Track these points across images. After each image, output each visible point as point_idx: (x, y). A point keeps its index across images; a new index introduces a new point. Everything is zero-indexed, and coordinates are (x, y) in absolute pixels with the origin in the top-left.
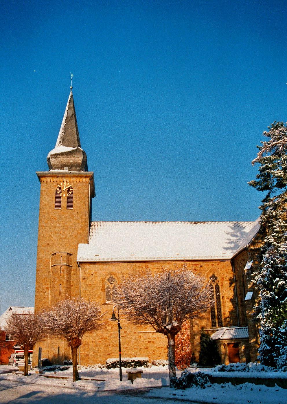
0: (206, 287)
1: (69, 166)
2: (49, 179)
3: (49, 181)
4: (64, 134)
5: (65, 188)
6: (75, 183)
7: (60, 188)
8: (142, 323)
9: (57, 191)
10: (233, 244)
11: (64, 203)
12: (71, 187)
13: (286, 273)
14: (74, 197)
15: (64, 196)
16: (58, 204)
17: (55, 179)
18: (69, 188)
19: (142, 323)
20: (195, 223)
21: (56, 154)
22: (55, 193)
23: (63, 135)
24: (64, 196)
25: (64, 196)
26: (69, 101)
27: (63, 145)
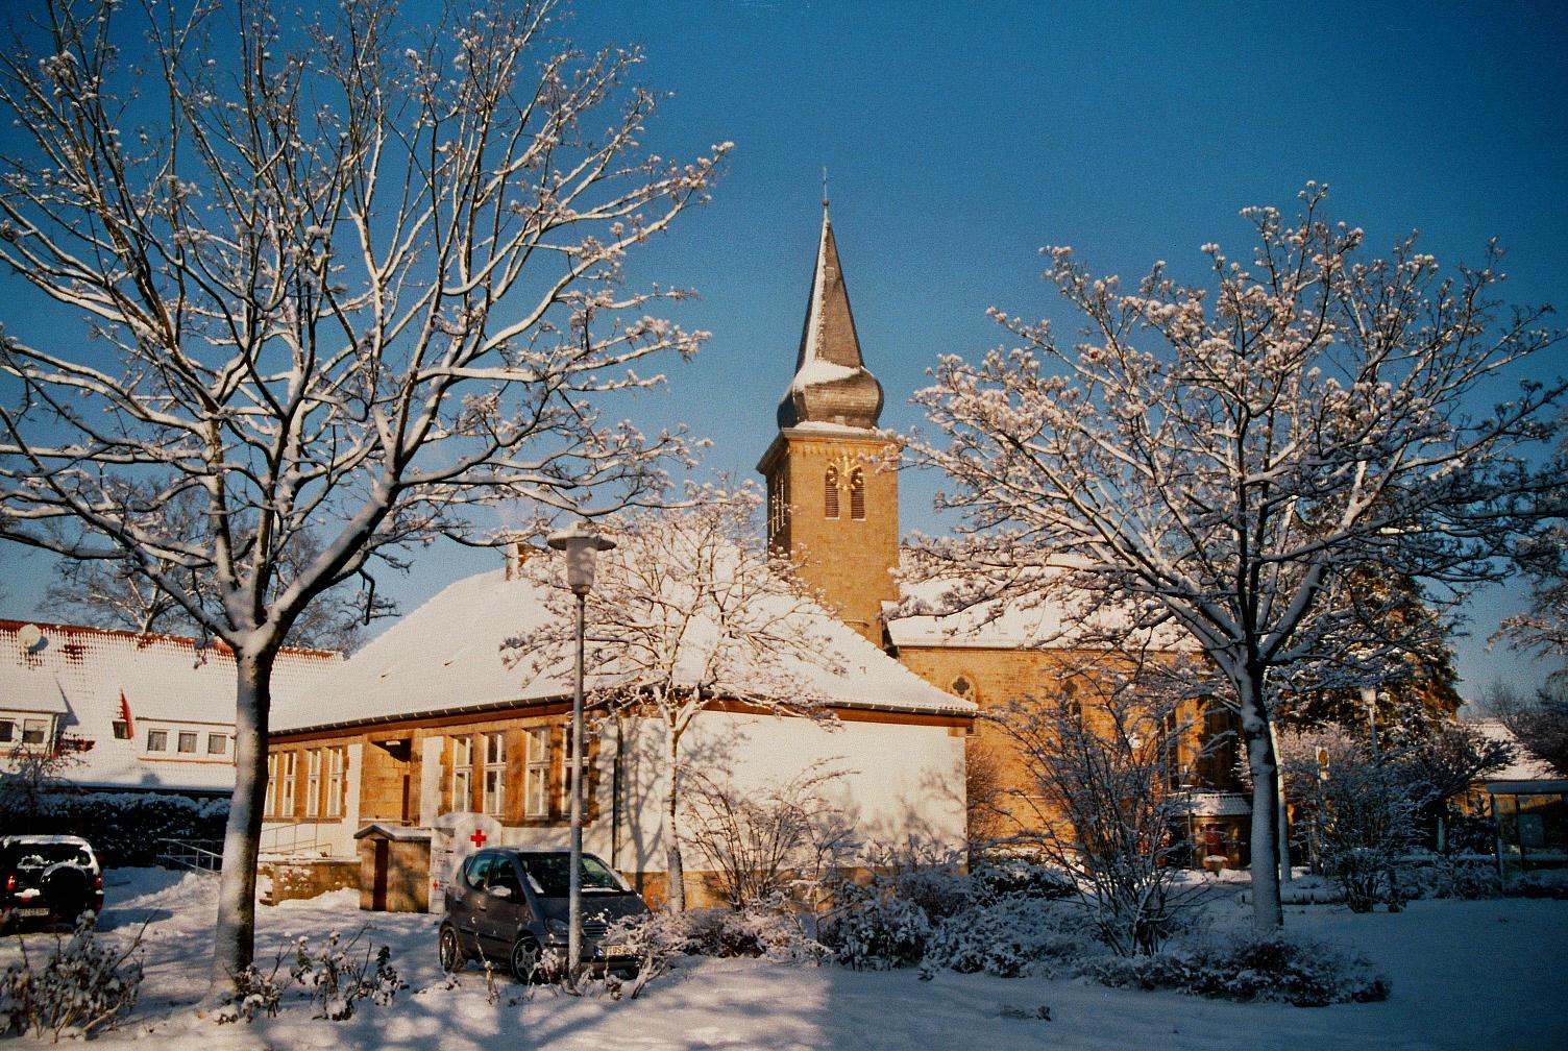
2: (809, 447)
4: (825, 328)
5: (847, 472)
7: (835, 470)
9: (828, 477)
11: (845, 505)
12: (860, 470)
14: (866, 492)
16: (832, 508)
17: (822, 447)
24: (845, 488)
25: (845, 488)
26: (827, 239)
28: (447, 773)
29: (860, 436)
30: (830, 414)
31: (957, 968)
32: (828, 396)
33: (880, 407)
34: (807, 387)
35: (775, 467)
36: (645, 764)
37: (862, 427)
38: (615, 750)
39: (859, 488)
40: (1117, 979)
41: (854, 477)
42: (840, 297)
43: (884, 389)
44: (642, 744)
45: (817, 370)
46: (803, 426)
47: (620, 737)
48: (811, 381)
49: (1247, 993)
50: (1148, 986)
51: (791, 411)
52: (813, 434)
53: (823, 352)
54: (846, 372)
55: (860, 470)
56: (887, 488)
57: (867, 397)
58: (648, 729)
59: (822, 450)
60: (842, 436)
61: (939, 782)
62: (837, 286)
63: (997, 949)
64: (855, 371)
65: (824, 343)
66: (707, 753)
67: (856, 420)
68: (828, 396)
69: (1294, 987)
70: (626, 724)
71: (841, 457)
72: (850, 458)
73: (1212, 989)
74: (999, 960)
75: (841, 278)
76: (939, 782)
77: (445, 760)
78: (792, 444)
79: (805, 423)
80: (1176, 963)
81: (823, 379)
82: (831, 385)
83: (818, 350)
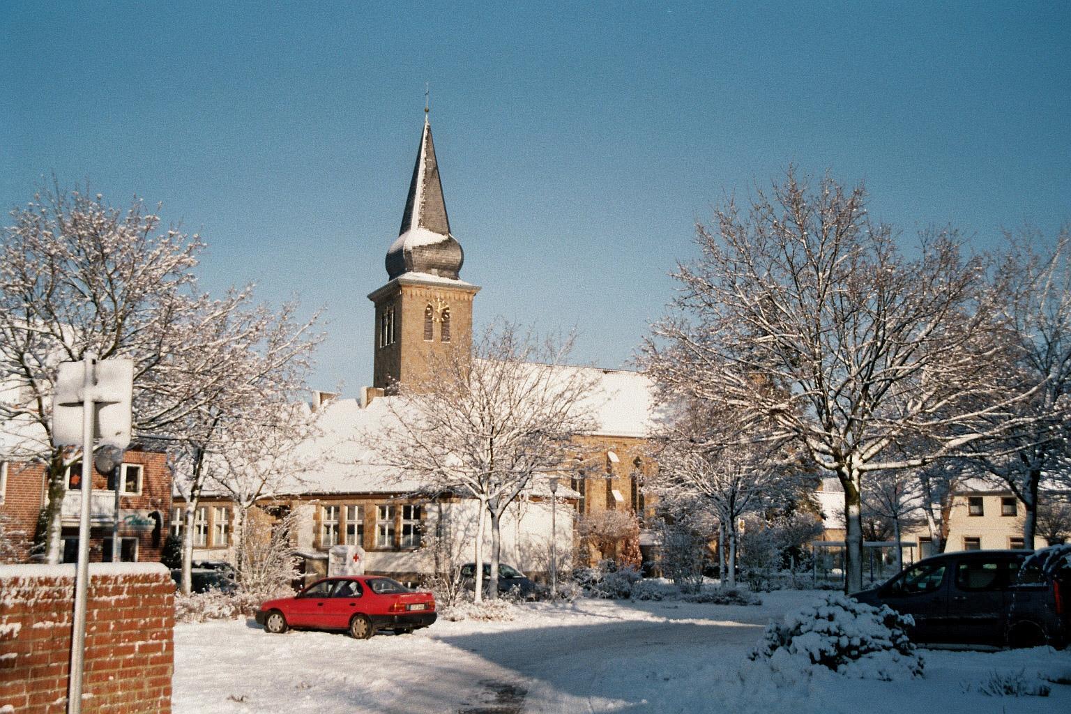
0: (273, 532)
1: (438, 268)
2: (415, 291)
3: (414, 294)
4: (425, 205)
5: (439, 310)
6: (453, 301)
7: (431, 307)
8: (1051, 348)
9: (427, 312)
10: (663, 414)
11: (437, 332)
12: (448, 309)
13: (1070, 534)
14: (451, 324)
15: (438, 320)
16: (429, 333)
17: (424, 291)
18: (445, 310)
19: (1051, 348)
20: (606, 372)
21: (420, 246)
22: (424, 314)
23: (423, 207)
24: (437, 319)
25: (438, 320)
26: (427, 138)
27: (426, 228)
28: (319, 525)
29: (449, 285)
30: (428, 267)
31: (642, 599)
32: (428, 255)
33: (461, 264)
34: (414, 248)
35: (387, 303)
36: (453, 525)
37: (449, 277)
38: (437, 517)
39: (447, 321)
40: (692, 600)
41: (444, 313)
42: (436, 181)
43: (464, 250)
44: (452, 516)
45: (419, 237)
46: (408, 276)
47: (440, 511)
48: (417, 244)
49: (727, 603)
50: (700, 602)
51: (397, 262)
52: (418, 282)
53: (422, 223)
54: (440, 238)
55: (448, 309)
56: (465, 322)
57: (452, 256)
58: (455, 506)
59: (423, 294)
60: (438, 284)
61: (562, 532)
62: (434, 173)
63: (655, 593)
64: (445, 237)
65: (424, 216)
66: (475, 519)
67: (445, 273)
68: (428, 255)
69: (739, 601)
70: (444, 506)
71: (436, 299)
72: (441, 300)
73: (718, 602)
74: (656, 596)
75: (436, 168)
76: (562, 532)
77: (316, 517)
78: (404, 289)
79: (411, 273)
80: (708, 596)
81: (425, 243)
82: (430, 247)
83: (420, 220)
